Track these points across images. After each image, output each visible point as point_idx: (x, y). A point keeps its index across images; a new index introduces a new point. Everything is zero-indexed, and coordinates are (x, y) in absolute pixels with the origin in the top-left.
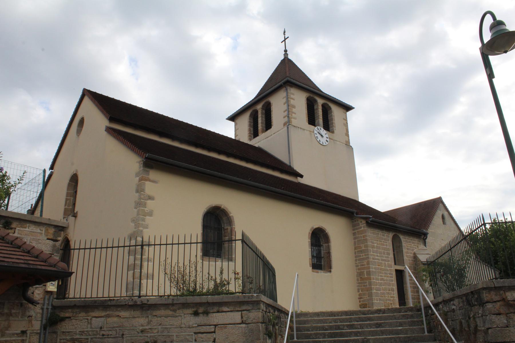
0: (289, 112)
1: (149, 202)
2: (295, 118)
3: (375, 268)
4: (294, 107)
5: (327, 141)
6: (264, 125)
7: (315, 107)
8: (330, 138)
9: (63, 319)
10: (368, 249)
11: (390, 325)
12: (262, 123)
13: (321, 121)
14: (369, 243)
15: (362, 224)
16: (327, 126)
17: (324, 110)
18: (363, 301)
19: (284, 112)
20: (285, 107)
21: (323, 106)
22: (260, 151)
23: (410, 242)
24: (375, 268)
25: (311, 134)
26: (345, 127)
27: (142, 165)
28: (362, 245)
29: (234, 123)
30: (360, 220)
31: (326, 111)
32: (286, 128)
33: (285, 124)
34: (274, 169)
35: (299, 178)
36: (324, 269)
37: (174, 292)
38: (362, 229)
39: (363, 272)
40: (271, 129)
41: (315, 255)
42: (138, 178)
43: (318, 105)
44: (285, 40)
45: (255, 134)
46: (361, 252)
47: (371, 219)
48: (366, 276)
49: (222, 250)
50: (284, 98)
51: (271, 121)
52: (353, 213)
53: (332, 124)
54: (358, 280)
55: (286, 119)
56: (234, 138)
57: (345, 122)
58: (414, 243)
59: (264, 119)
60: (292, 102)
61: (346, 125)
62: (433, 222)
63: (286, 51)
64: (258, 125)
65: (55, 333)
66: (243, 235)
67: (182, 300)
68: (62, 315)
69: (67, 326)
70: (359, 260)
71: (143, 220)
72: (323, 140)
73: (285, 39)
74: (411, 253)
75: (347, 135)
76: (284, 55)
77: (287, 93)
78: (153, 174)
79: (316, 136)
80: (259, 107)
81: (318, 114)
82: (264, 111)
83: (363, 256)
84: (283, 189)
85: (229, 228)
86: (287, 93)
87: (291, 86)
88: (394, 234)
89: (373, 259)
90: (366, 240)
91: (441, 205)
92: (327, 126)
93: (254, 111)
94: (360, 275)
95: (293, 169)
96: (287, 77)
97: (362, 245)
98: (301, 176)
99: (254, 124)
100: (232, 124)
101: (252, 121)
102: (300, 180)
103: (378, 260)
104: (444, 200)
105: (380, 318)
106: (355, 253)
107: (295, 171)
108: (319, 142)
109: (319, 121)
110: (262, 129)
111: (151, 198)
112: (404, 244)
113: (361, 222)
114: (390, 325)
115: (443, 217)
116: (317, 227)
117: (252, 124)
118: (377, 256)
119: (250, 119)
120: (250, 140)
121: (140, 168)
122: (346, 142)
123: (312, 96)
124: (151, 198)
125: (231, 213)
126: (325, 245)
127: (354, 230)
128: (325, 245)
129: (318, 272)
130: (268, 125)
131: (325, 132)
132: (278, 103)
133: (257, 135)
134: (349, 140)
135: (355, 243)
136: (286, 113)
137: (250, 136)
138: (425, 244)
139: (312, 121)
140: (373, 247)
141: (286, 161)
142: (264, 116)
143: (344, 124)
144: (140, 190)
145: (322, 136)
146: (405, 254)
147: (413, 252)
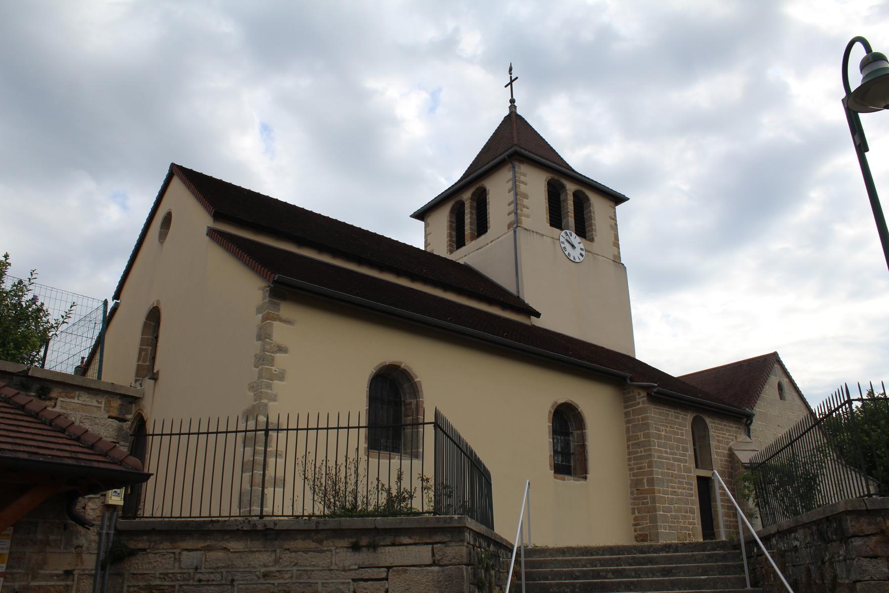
0: (517, 205)
1: (279, 356)
2: (528, 216)
4: (526, 196)
5: (581, 254)
6: (475, 227)
8: (586, 251)
9: (133, 553)
10: (649, 441)
11: (687, 571)
12: (471, 223)
13: (571, 220)
15: (641, 398)
16: (583, 229)
17: (579, 202)
18: (640, 530)
19: (509, 214)
20: (511, 197)
21: (576, 194)
22: (466, 269)
23: (722, 429)
30: (636, 391)
31: (581, 204)
32: (512, 232)
33: (509, 226)
34: (491, 302)
35: (533, 318)
36: (575, 474)
37: (319, 509)
38: (641, 405)
41: (559, 449)
42: (260, 316)
43: (566, 195)
44: (511, 84)
45: (458, 241)
46: (638, 445)
47: (655, 390)
48: (646, 487)
49: (400, 439)
52: (624, 378)
54: (632, 493)
55: (512, 217)
56: (423, 248)
57: (614, 222)
58: (729, 431)
59: (475, 216)
60: (522, 188)
61: (615, 228)
63: (512, 101)
65: (120, 575)
66: (437, 414)
67: (332, 524)
68: (132, 545)
70: (635, 459)
71: (269, 387)
72: (575, 254)
73: (512, 81)
74: (724, 449)
75: (616, 244)
76: (510, 107)
78: (286, 310)
79: (563, 246)
80: (467, 196)
82: (475, 204)
83: (641, 452)
84: (506, 337)
85: (414, 401)
87: (522, 162)
89: (659, 457)
90: (647, 426)
92: (583, 229)
93: (457, 203)
94: (636, 485)
95: (523, 302)
96: (515, 145)
98: (538, 315)
101: (454, 220)
102: (535, 321)
103: (668, 459)
105: (669, 560)
106: (628, 447)
107: (527, 305)
108: (568, 257)
109: (568, 222)
110: (472, 234)
111: (281, 349)
112: (712, 433)
113: (639, 394)
114: (687, 571)
115: (780, 387)
116: (563, 401)
118: (666, 452)
120: (451, 252)
121: (264, 298)
122: (614, 256)
124: (281, 349)
125: (417, 377)
126: (576, 433)
127: (626, 407)
128: (576, 433)
129: (564, 479)
130: (482, 227)
131: (578, 239)
132: (498, 190)
133: (464, 245)
134: (619, 253)
136: (512, 207)
137: (450, 245)
139: (556, 221)
140: (659, 437)
141: (511, 288)
142: (474, 212)
143: (611, 226)
144: (263, 335)
145: (573, 246)
146: (713, 450)
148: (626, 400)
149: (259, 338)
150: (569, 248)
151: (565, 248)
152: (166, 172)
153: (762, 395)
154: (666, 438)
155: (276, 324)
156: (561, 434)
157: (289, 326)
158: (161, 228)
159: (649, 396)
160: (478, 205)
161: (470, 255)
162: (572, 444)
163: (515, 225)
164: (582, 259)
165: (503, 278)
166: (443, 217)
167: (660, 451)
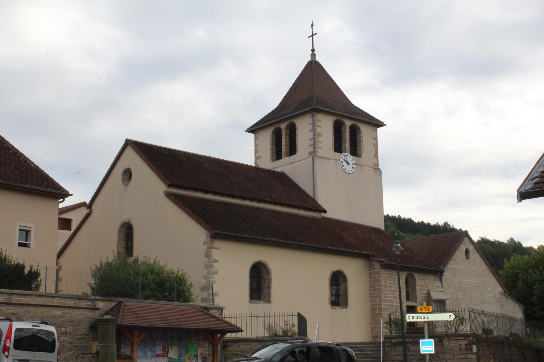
0: (314, 141)
1: (215, 264)
2: (320, 127)
4: (320, 135)
5: (353, 168)
7: (343, 130)
8: (357, 164)
9: (228, 346)
10: (380, 289)
11: (367, 351)
12: (286, 145)
13: (347, 145)
14: (383, 283)
15: (377, 266)
16: (355, 151)
17: (353, 129)
19: (310, 140)
20: (311, 135)
23: (425, 279)
25: (336, 163)
27: (209, 237)
30: (375, 262)
31: (354, 131)
32: (311, 159)
33: (310, 154)
36: (342, 305)
37: (269, 335)
38: (377, 270)
40: (296, 155)
41: (334, 293)
42: (206, 246)
43: (345, 129)
45: (277, 155)
46: (375, 290)
47: (384, 263)
48: (378, 312)
49: (261, 294)
53: (360, 146)
54: (371, 315)
55: (311, 149)
57: (375, 141)
58: (429, 280)
59: (288, 140)
60: (318, 130)
61: (376, 145)
62: (453, 257)
63: (313, 50)
65: (225, 351)
67: (271, 339)
68: (227, 344)
70: (373, 297)
71: (213, 278)
72: (349, 168)
74: (425, 290)
75: (376, 156)
77: (314, 120)
78: (217, 243)
79: (342, 164)
81: (345, 138)
82: (288, 131)
83: (376, 293)
85: (267, 277)
86: (314, 120)
88: (408, 273)
89: (385, 297)
90: (379, 281)
91: (466, 239)
92: (355, 151)
93: (276, 128)
94: (373, 310)
100: (252, 135)
101: (274, 139)
102: (323, 214)
103: (390, 297)
104: (470, 233)
105: (363, 347)
106: (370, 291)
109: (345, 146)
112: (418, 282)
114: (367, 351)
115: (467, 251)
117: (275, 142)
118: (389, 294)
119: (272, 136)
121: (207, 238)
123: (339, 118)
124: (216, 261)
126: (343, 285)
127: (370, 270)
128: (343, 285)
129: (335, 309)
130: (293, 150)
131: (352, 157)
132: (303, 127)
133: (281, 158)
134: (378, 162)
135: (370, 281)
136: (312, 142)
137: (272, 156)
138: (441, 281)
139: (338, 148)
140: (386, 286)
141: (311, 194)
142: (288, 137)
144: (208, 255)
145: (348, 163)
147: (427, 289)
149: (206, 256)
150: (345, 163)
151: (343, 165)
155: (214, 250)
156: (335, 285)
157: (218, 250)
158: (123, 175)
159: (381, 265)
160: (290, 132)
161: (284, 166)
162: (340, 291)
163: (313, 154)
164: (353, 170)
165: (304, 184)
166: (267, 136)
167: (386, 294)
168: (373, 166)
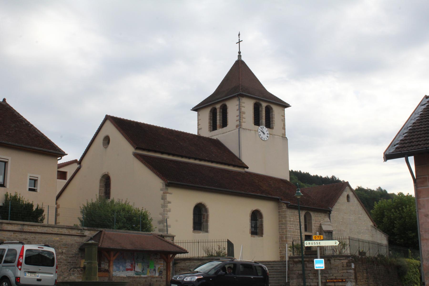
0: (240, 117)
1: (169, 204)
2: (245, 122)
3: (291, 235)
5: (267, 137)
7: (260, 109)
8: (270, 134)
9: (177, 263)
11: (276, 267)
13: (264, 121)
15: (284, 206)
16: (269, 125)
18: (282, 254)
19: (237, 116)
20: (237, 113)
23: (318, 216)
24: (291, 235)
25: (255, 133)
26: (282, 123)
28: (283, 220)
29: (197, 112)
30: (283, 204)
31: (269, 111)
33: (237, 126)
37: (206, 255)
39: (283, 237)
42: (162, 192)
43: (262, 108)
45: (214, 127)
46: (282, 224)
50: (237, 105)
51: (227, 121)
53: (273, 121)
54: (280, 241)
55: (238, 123)
58: (321, 217)
59: (221, 116)
60: (243, 109)
61: (284, 120)
63: (240, 53)
64: (216, 121)
67: (207, 258)
69: (179, 265)
70: (281, 229)
71: (167, 214)
72: (264, 137)
75: (284, 128)
78: (170, 190)
79: (259, 134)
82: (221, 110)
83: (283, 226)
85: (206, 214)
86: (240, 102)
89: (290, 229)
90: (286, 217)
91: (347, 187)
92: (269, 125)
97: (283, 220)
98: (247, 168)
99: (213, 118)
100: (196, 113)
101: (212, 115)
102: (246, 170)
105: (273, 264)
108: (261, 139)
109: (262, 121)
110: (220, 125)
111: (169, 202)
114: (276, 267)
115: (348, 197)
119: (210, 114)
121: (163, 186)
123: (258, 101)
124: (169, 202)
127: (279, 209)
130: (224, 124)
131: (266, 129)
132: (232, 107)
133: (216, 129)
134: (285, 132)
135: (279, 218)
136: (238, 118)
137: (210, 128)
139: (257, 122)
142: (221, 114)
143: (282, 120)
144: (164, 198)
146: (313, 225)
148: (279, 207)
149: (162, 199)
150: (261, 133)
152: (103, 117)
153: (339, 201)
154: (293, 221)
155: (168, 195)
156: (254, 220)
159: (287, 206)
161: (218, 135)
163: (239, 126)
164: (267, 138)
166: (206, 113)
167: (290, 226)
168: (281, 135)
